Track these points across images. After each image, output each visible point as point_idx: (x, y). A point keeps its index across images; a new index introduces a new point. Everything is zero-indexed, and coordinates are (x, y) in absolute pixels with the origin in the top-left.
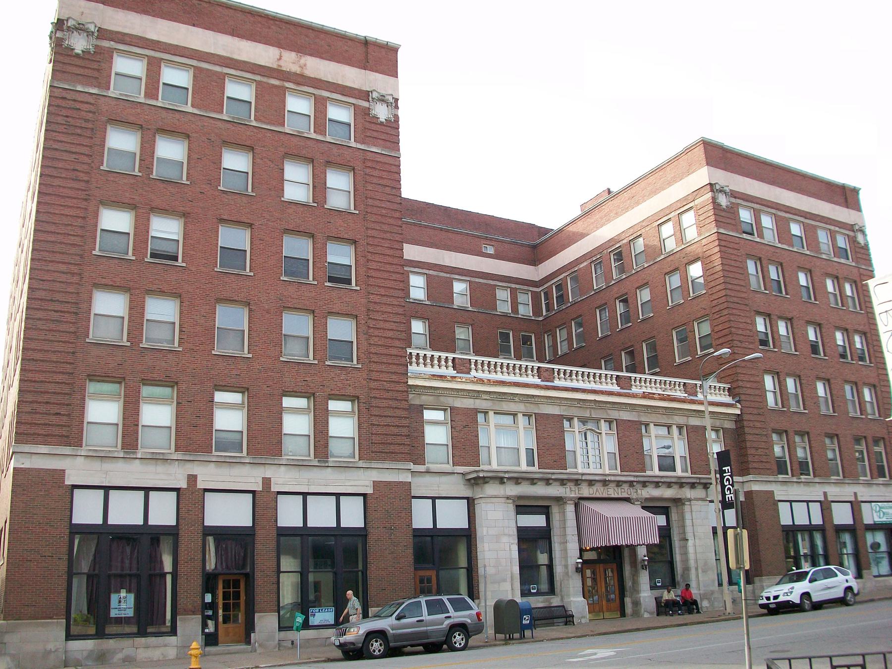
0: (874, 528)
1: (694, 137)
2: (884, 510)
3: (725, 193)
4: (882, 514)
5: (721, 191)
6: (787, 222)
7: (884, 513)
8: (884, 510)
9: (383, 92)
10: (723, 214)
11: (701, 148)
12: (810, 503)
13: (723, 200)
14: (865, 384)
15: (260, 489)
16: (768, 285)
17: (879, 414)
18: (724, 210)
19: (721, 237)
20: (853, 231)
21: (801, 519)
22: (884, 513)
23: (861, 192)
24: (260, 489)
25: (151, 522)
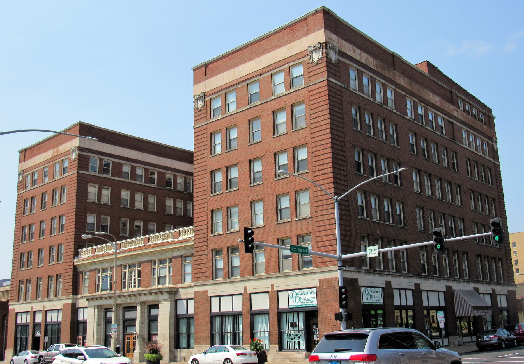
0: (291, 311)
1: (318, 6)
2: (300, 296)
3: (336, 51)
4: (369, 296)
5: (333, 48)
6: (404, 98)
7: (300, 299)
8: (371, 294)
9: (313, 45)
10: (331, 66)
11: (321, 15)
12: (407, 291)
13: (333, 57)
14: (398, 201)
15: (244, 293)
16: (388, 138)
17: (380, 218)
18: (333, 64)
19: (330, 85)
20: (492, 141)
21: (226, 308)
22: (371, 296)
23: (495, 119)
24: (244, 293)
25: (441, 305)
